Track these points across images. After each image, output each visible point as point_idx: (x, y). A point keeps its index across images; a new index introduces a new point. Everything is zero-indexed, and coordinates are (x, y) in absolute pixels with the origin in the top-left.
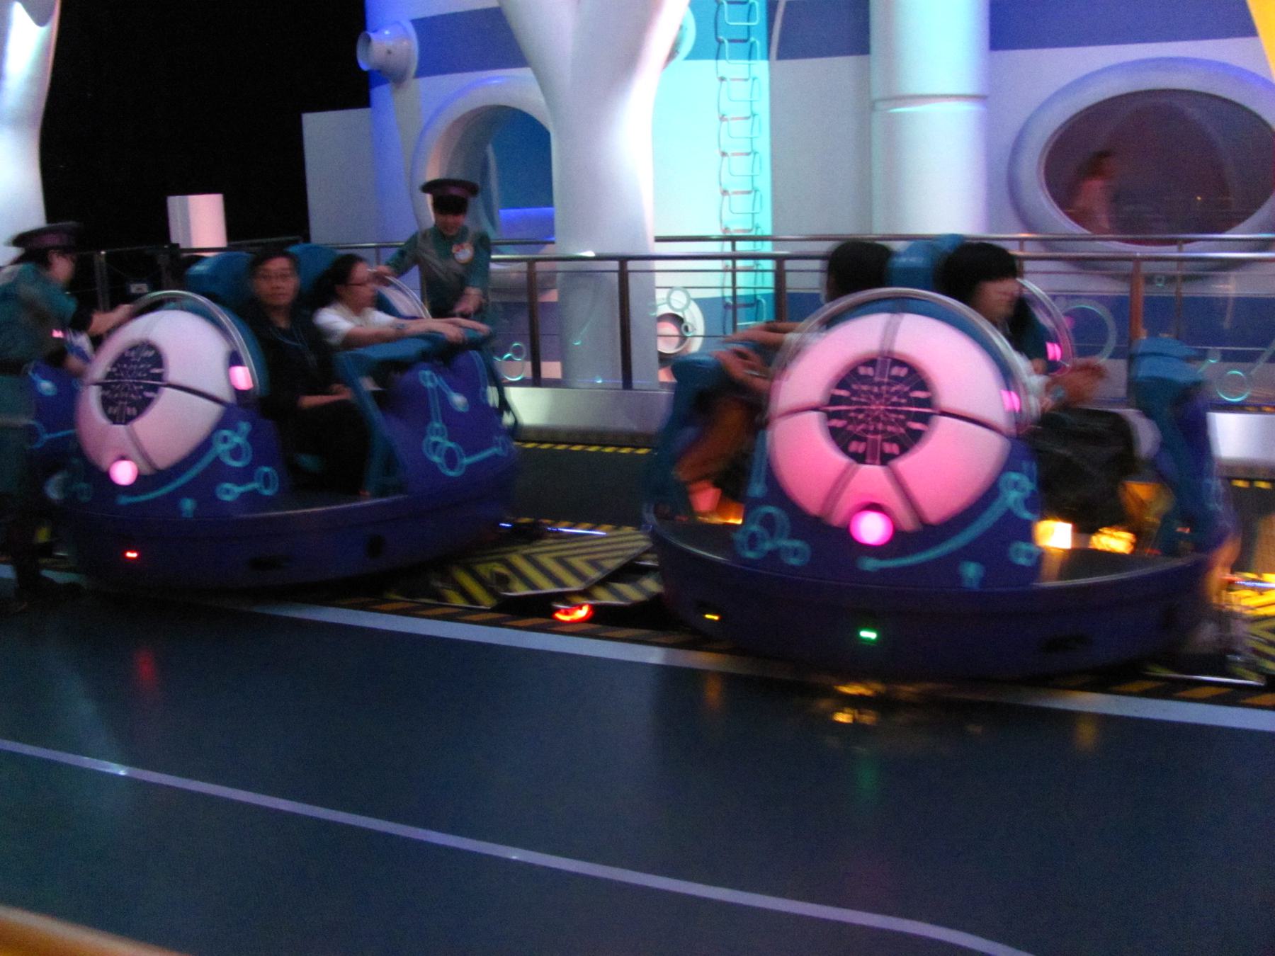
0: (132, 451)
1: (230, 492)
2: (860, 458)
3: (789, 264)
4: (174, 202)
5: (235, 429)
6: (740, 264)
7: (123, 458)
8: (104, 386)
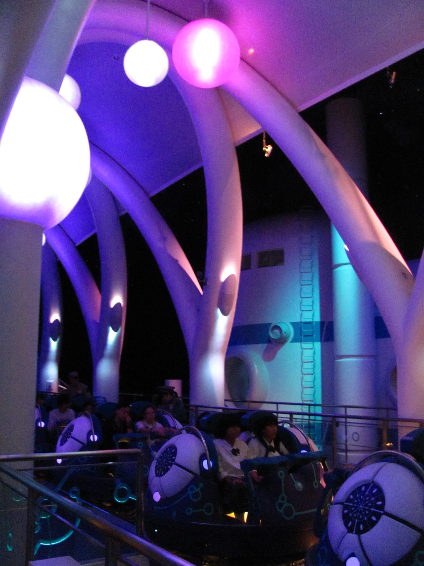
0: (358, 551)
1: (190, 511)
2: (350, 530)
3: (295, 416)
4: (166, 381)
5: (197, 487)
6: (349, 420)
7: (353, 555)
8: (158, 462)
